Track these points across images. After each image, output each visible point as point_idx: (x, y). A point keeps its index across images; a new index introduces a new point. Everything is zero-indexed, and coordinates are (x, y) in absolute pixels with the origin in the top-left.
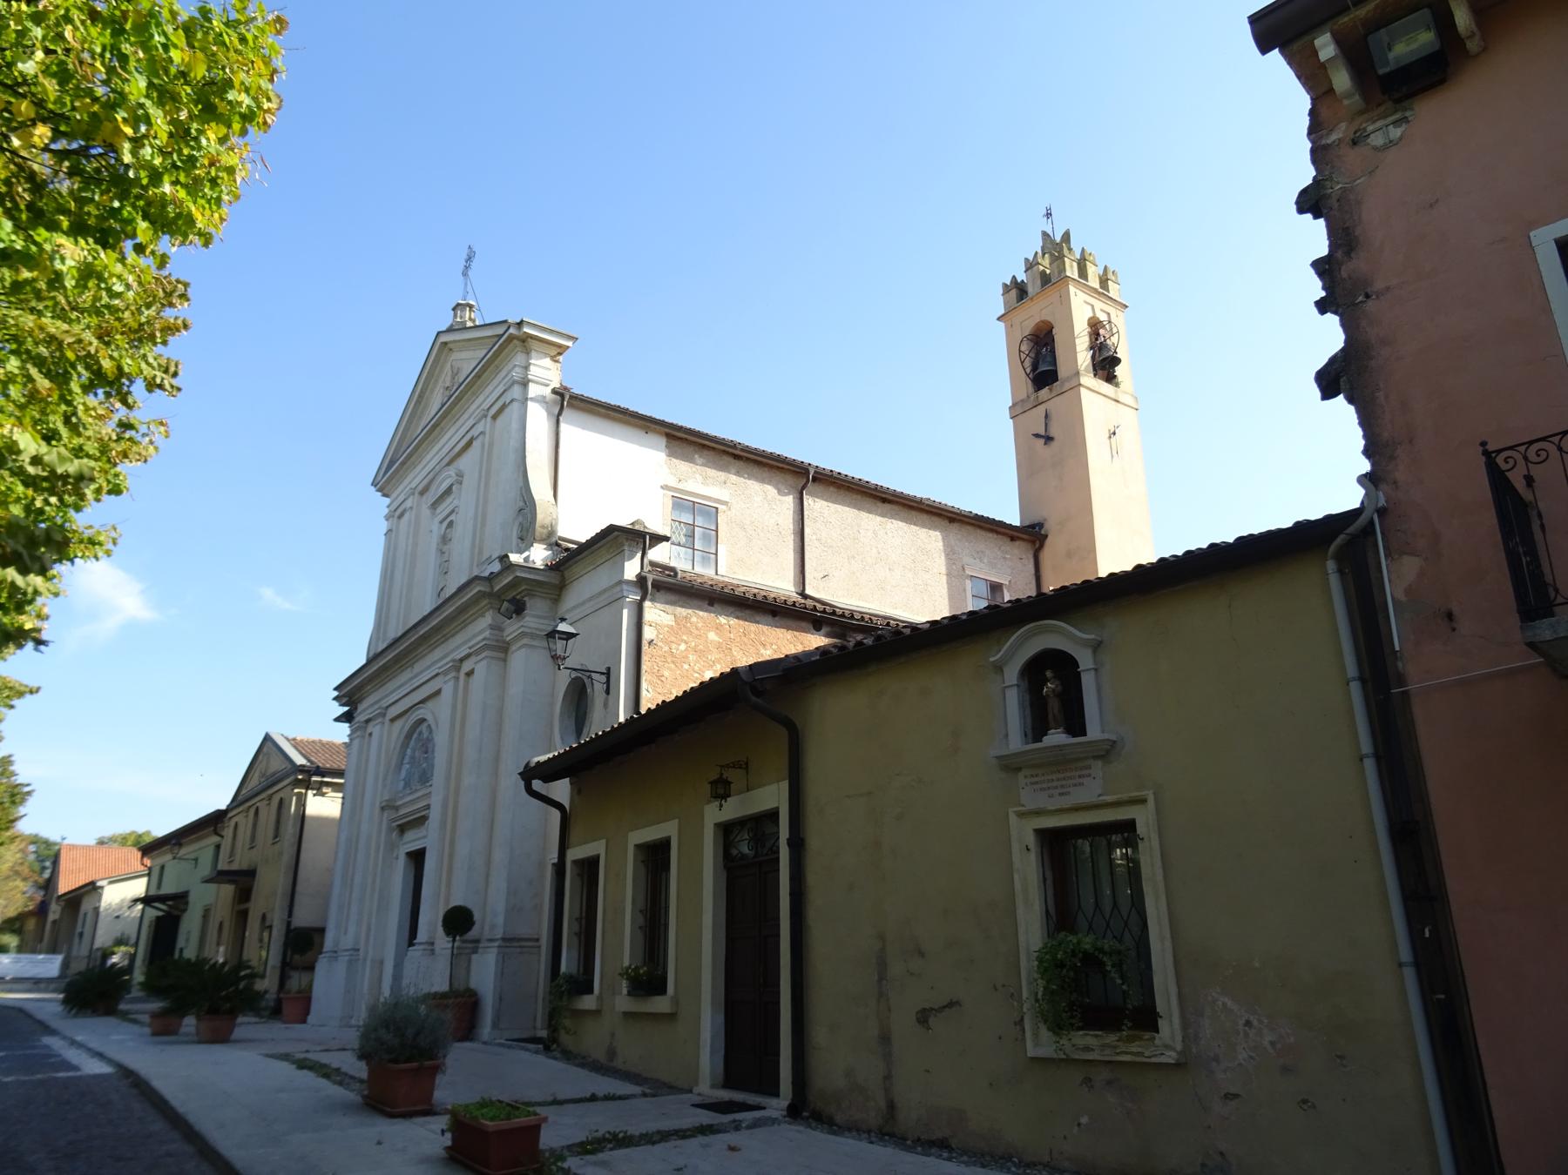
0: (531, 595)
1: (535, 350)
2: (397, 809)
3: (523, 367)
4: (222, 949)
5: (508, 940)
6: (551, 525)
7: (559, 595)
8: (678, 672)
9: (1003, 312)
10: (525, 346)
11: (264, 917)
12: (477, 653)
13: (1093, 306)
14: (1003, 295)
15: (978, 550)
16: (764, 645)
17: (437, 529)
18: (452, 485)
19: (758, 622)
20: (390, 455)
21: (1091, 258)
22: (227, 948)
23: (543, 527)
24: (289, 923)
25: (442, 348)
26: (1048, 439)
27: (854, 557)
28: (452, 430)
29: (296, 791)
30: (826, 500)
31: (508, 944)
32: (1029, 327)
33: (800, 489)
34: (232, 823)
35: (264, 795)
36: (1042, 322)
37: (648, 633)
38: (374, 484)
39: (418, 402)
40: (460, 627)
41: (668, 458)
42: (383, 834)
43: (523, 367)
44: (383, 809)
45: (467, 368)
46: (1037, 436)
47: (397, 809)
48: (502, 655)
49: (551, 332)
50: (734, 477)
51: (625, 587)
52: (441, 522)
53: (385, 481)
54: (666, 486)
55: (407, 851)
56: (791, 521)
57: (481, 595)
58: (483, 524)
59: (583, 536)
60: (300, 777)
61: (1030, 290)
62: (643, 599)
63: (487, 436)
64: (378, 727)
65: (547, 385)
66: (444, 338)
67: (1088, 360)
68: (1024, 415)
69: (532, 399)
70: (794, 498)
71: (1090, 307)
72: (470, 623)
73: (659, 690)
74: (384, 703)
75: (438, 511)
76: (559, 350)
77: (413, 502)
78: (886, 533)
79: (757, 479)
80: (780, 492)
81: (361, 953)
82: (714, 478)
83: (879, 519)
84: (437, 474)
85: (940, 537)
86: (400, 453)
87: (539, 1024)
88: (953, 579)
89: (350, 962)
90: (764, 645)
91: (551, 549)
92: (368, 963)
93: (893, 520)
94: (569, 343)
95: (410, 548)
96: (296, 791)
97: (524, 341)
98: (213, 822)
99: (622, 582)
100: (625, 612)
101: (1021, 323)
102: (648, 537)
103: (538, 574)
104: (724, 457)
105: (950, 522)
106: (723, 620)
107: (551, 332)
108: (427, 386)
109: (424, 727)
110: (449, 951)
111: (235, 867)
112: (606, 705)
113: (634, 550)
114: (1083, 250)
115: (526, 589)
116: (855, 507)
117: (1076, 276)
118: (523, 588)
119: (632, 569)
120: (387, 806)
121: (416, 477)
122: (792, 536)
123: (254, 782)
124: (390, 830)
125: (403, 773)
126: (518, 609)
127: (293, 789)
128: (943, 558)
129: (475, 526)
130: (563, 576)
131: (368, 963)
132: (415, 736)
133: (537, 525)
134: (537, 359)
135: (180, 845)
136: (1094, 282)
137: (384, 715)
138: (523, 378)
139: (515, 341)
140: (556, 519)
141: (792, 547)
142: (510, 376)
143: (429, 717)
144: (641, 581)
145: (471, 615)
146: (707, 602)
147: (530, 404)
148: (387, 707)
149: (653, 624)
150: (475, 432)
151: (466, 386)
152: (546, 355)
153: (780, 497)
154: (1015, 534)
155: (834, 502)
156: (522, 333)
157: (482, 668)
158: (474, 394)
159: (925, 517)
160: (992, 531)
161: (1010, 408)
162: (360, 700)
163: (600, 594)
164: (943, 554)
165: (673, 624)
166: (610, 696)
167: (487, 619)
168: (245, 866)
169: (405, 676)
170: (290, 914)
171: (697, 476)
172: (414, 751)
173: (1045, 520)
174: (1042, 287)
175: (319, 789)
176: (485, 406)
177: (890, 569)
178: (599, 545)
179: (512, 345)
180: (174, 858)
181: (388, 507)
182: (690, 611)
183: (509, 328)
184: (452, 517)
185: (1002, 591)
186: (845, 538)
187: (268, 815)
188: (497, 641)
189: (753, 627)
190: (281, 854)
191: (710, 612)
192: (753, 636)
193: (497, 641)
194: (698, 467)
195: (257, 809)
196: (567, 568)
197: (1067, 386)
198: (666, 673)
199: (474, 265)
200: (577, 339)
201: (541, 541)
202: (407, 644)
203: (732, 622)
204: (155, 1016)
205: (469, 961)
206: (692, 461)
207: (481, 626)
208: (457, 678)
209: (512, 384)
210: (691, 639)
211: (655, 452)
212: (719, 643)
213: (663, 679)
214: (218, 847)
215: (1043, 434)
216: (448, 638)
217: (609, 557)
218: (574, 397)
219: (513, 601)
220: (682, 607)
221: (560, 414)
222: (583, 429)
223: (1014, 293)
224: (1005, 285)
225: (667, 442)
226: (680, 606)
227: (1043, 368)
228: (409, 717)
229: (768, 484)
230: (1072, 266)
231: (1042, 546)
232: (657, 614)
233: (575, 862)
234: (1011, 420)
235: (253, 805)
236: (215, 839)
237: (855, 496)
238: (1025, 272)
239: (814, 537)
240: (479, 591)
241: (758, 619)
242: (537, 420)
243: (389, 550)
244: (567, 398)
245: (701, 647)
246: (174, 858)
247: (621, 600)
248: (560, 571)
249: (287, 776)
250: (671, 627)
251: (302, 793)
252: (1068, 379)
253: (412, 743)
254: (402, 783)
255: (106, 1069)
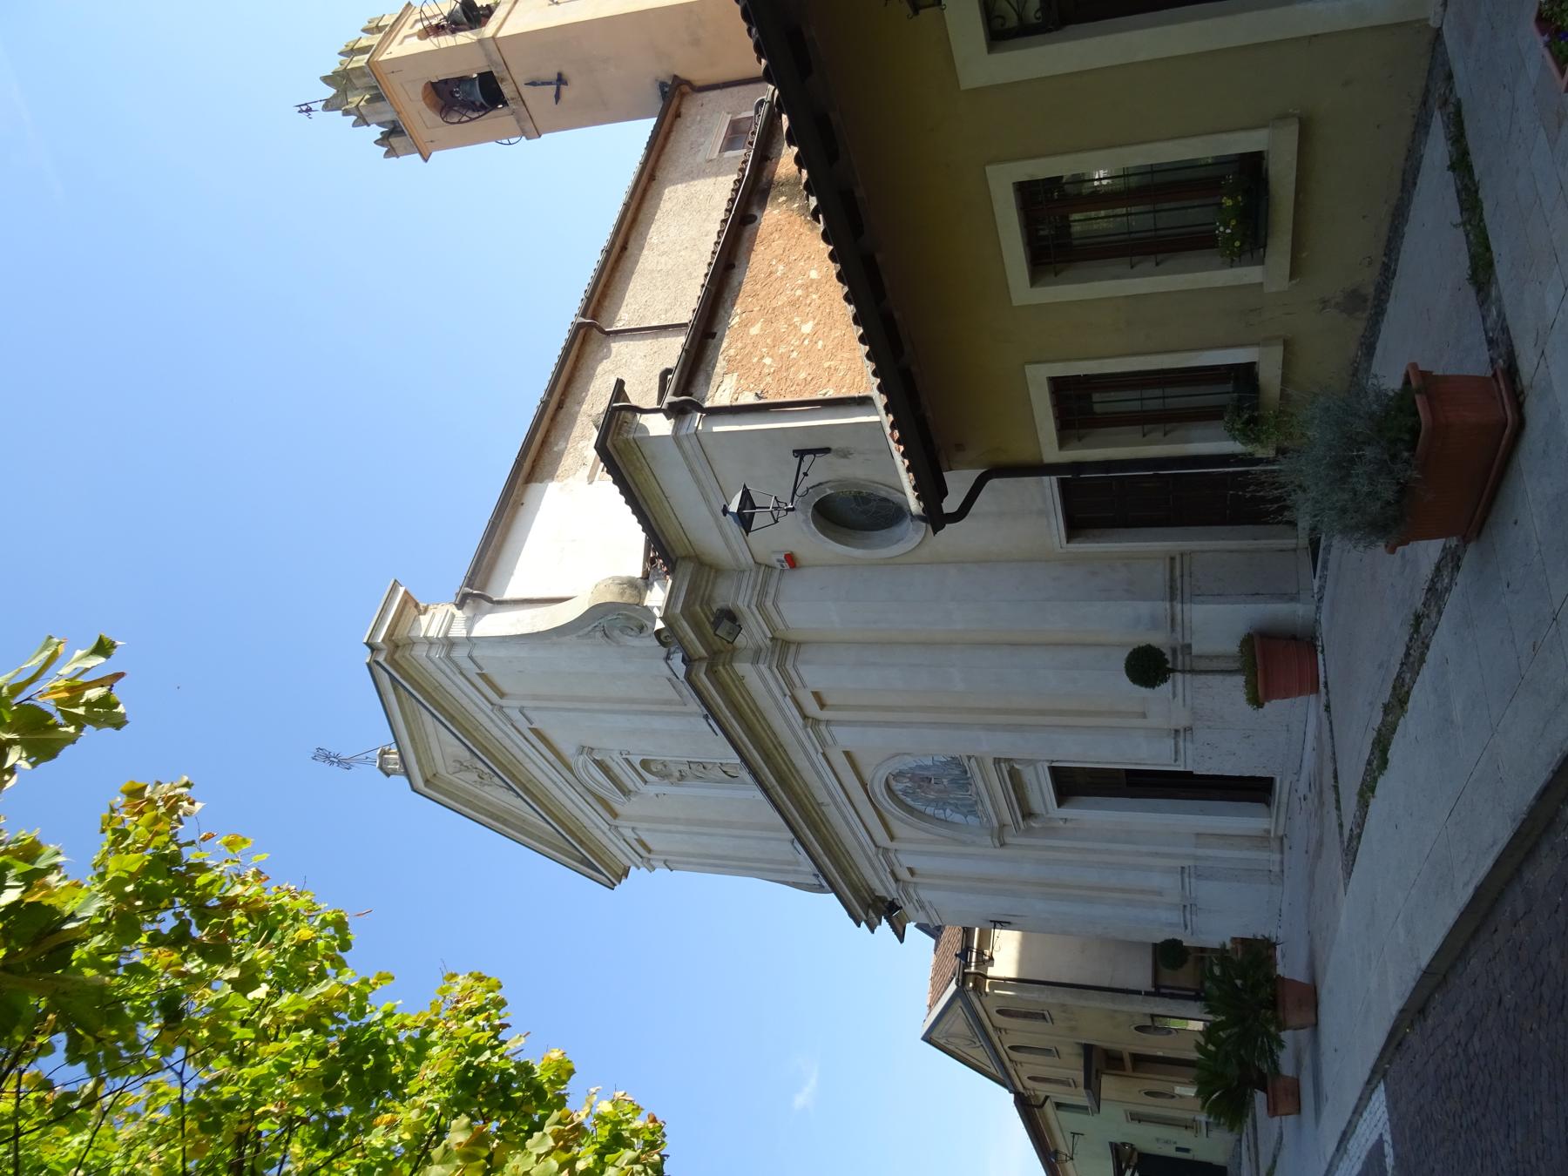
0: (707, 602)
1: (409, 632)
2: (1002, 826)
3: (430, 648)
4: (1179, 1090)
5: (1173, 592)
6: (620, 584)
7: (711, 567)
8: (801, 363)
9: (417, 156)
10: (404, 645)
11: (1140, 1029)
12: (790, 684)
13: (406, 37)
14: (398, 157)
15: (688, 149)
16: (771, 273)
17: (655, 787)
18: (596, 761)
19: (740, 284)
20: (575, 864)
21: (352, 44)
22: (1179, 1083)
23: (622, 594)
24: (1148, 994)
25: (432, 786)
26: (561, 80)
27: (690, 274)
28: (530, 766)
29: (987, 990)
30: (619, 308)
31: (1179, 592)
32: (431, 117)
33: (604, 336)
34: (1030, 1084)
35: (996, 1040)
36: (424, 99)
37: (748, 399)
38: (612, 886)
39: (505, 822)
40: (762, 722)
41: (555, 479)
42: (1032, 841)
43: (430, 648)
44: (1003, 844)
45: (454, 748)
46: (557, 97)
47: (1002, 826)
48: (793, 648)
49: (384, 610)
50: (584, 406)
51: (683, 432)
52: (646, 782)
53: (612, 875)
54: (589, 477)
55: (1056, 806)
56: (641, 342)
57: (712, 672)
58: (633, 701)
59: (634, 537)
60: (971, 985)
61: (389, 117)
62: (700, 409)
63: (525, 703)
64: (900, 856)
65: (453, 616)
66: (420, 784)
67: (468, 34)
68: (534, 118)
69: (469, 632)
70: (615, 342)
71: (407, 40)
72: (755, 703)
73: (825, 381)
74: (871, 849)
75: (631, 786)
76: (411, 605)
77: (626, 827)
78: (663, 243)
79: (588, 383)
80: (607, 357)
81: (1186, 863)
82: (584, 429)
83: (645, 252)
84: (588, 789)
85: (672, 188)
86: (578, 854)
87: (1289, 543)
88: (722, 170)
89: (1198, 877)
90: (771, 273)
91: (652, 584)
92: (1200, 852)
93: (649, 237)
94: (402, 590)
95: (681, 828)
96: (987, 990)
97: (397, 646)
98: (1028, 1108)
99: (676, 436)
100: (716, 429)
101: (427, 128)
102: (615, 405)
103: (679, 589)
104: (559, 419)
105: (654, 180)
106: (735, 321)
107: (384, 610)
108: (484, 809)
109: (897, 787)
110: (1188, 676)
111: (1080, 1076)
112: (845, 454)
113: (634, 426)
114: (340, 54)
115: (701, 606)
116: (629, 278)
117: (367, 56)
118: (699, 610)
119: (659, 426)
120: (999, 839)
121: (592, 820)
122: (660, 339)
123: (980, 1055)
124: (1029, 831)
125: (958, 818)
126: (730, 617)
127: (986, 994)
128: (696, 182)
129: (636, 713)
130: (684, 558)
131: (1200, 852)
132: (909, 801)
133: (621, 601)
134: (421, 629)
135: (1056, 1152)
136: (375, 39)
137: (886, 850)
138: (444, 645)
139: (397, 656)
140: (614, 579)
141: (673, 339)
142: (437, 661)
143: (882, 774)
144: (676, 412)
145: (743, 697)
146: (710, 340)
147: (475, 633)
148: (876, 846)
149: (735, 397)
150: (523, 725)
151: (466, 738)
152: (416, 619)
153: (612, 356)
154: (672, 111)
155: (622, 298)
156: (383, 646)
157: (813, 675)
158: (477, 729)
159: (646, 205)
160: (667, 138)
161: (528, 139)
162: (871, 891)
163: (697, 481)
164: (691, 183)
165: (736, 374)
166: (834, 447)
167: (743, 668)
168: (1080, 1062)
169: (832, 813)
170: (1139, 993)
171: (580, 446)
172: (928, 802)
173: (656, 80)
174: (384, 100)
175: (985, 961)
176: (487, 707)
177: (706, 235)
178: (632, 486)
179: (401, 662)
180: (1072, 1159)
181: (639, 868)
182: (721, 358)
183: (378, 663)
184: (636, 761)
185: (739, 121)
186: (667, 284)
187: (1020, 1031)
188: (773, 652)
189: (747, 287)
190: (1064, 1007)
191: (724, 335)
192: (758, 286)
193: (773, 652)
194: (569, 446)
195: (1011, 1048)
196: (673, 550)
197: (496, 57)
198: (802, 375)
199: (334, 750)
200: (396, 581)
201: (641, 596)
202: (790, 805)
203: (739, 311)
204: (1273, 1110)
205: (1200, 657)
206: (560, 455)
207: (755, 678)
208: (828, 722)
209: (451, 659)
210: (758, 352)
211: (546, 494)
212: (764, 322)
213: (809, 378)
214: (1059, 1106)
215: (555, 86)
216: (779, 743)
217: (647, 470)
218: (470, 582)
219: (716, 625)
220: (714, 367)
221: (490, 600)
222: (512, 574)
223: (394, 140)
224: (387, 155)
225: (536, 482)
226: (713, 368)
227: (478, 96)
228: (885, 808)
229: (595, 371)
230: (358, 61)
231: (688, 83)
232: (721, 392)
233: (1063, 443)
234: (543, 136)
235: (1006, 1053)
236: (1049, 1107)
237: (617, 278)
238: (369, 125)
239: (663, 316)
240: (705, 674)
241: (736, 283)
242: (493, 624)
243: (688, 863)
244: (468, 590)
245: (768, 341)
246: (1072, 1159)
247: (699, 436)
248: (676, 561)
249: (969, 1006)
250: (740, 377)
251: (990, 984)
252: (488, 56)
253: (918, 805)
254: (970, 818)
255: (1379, 1098)
